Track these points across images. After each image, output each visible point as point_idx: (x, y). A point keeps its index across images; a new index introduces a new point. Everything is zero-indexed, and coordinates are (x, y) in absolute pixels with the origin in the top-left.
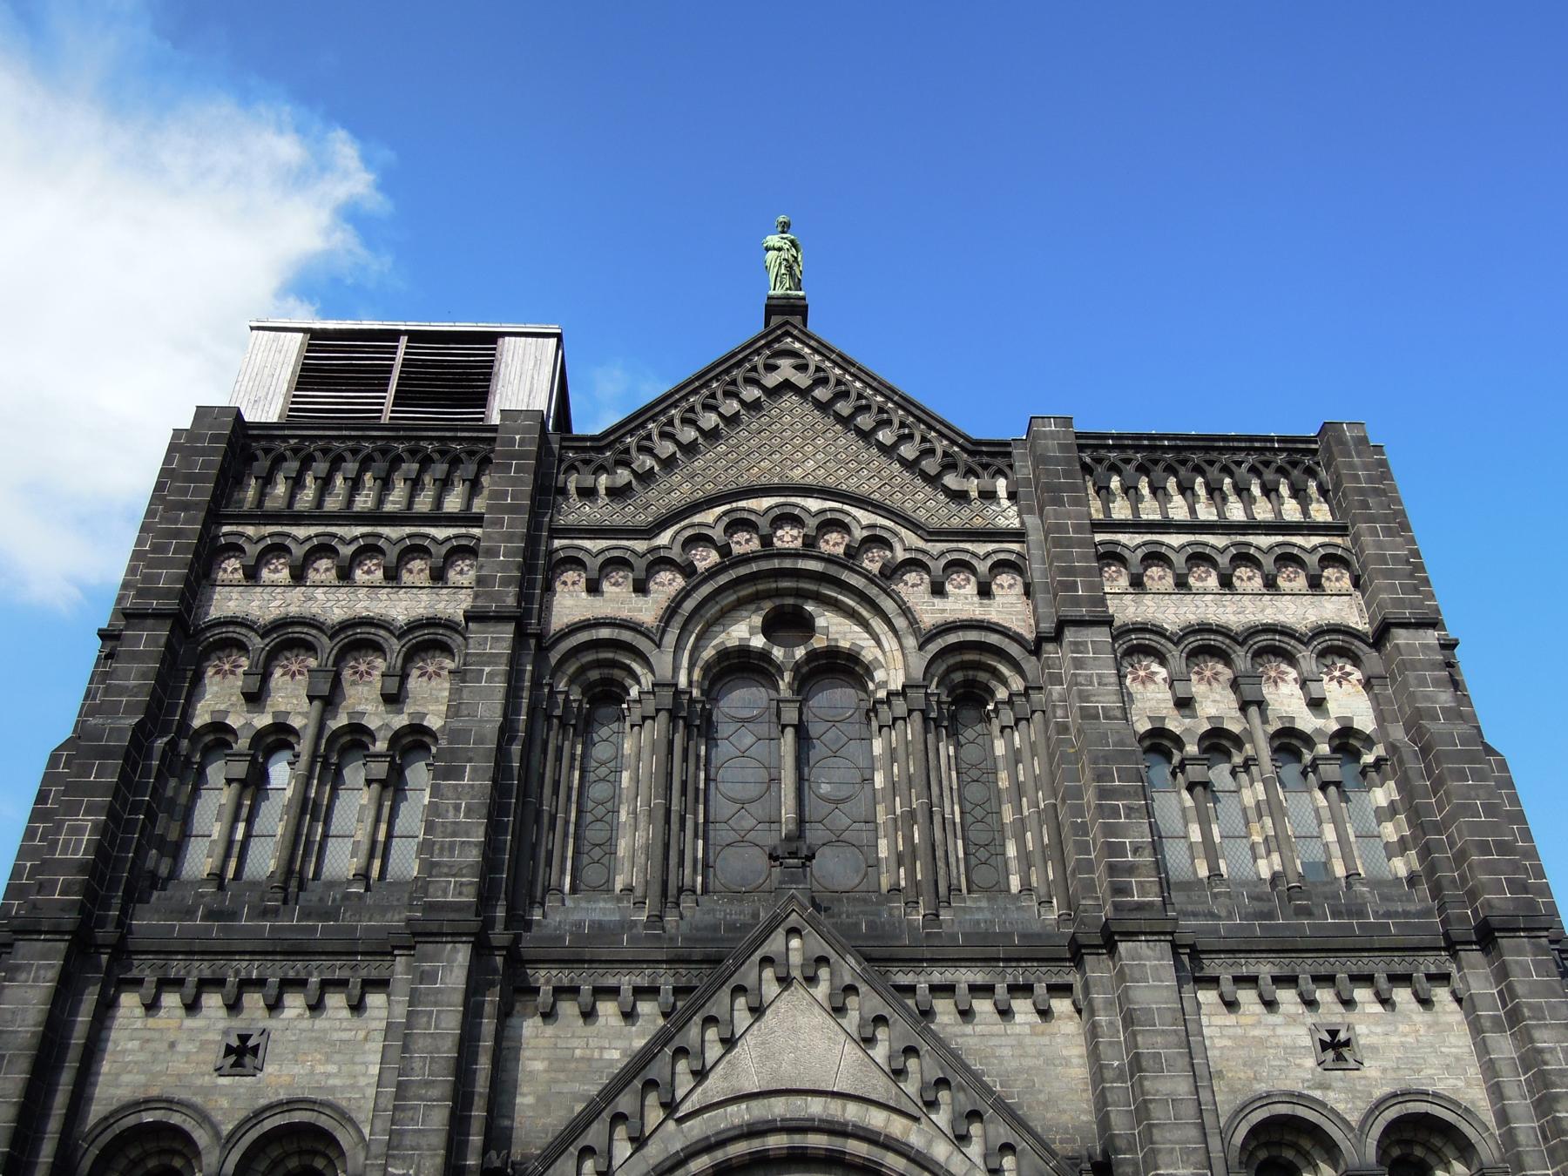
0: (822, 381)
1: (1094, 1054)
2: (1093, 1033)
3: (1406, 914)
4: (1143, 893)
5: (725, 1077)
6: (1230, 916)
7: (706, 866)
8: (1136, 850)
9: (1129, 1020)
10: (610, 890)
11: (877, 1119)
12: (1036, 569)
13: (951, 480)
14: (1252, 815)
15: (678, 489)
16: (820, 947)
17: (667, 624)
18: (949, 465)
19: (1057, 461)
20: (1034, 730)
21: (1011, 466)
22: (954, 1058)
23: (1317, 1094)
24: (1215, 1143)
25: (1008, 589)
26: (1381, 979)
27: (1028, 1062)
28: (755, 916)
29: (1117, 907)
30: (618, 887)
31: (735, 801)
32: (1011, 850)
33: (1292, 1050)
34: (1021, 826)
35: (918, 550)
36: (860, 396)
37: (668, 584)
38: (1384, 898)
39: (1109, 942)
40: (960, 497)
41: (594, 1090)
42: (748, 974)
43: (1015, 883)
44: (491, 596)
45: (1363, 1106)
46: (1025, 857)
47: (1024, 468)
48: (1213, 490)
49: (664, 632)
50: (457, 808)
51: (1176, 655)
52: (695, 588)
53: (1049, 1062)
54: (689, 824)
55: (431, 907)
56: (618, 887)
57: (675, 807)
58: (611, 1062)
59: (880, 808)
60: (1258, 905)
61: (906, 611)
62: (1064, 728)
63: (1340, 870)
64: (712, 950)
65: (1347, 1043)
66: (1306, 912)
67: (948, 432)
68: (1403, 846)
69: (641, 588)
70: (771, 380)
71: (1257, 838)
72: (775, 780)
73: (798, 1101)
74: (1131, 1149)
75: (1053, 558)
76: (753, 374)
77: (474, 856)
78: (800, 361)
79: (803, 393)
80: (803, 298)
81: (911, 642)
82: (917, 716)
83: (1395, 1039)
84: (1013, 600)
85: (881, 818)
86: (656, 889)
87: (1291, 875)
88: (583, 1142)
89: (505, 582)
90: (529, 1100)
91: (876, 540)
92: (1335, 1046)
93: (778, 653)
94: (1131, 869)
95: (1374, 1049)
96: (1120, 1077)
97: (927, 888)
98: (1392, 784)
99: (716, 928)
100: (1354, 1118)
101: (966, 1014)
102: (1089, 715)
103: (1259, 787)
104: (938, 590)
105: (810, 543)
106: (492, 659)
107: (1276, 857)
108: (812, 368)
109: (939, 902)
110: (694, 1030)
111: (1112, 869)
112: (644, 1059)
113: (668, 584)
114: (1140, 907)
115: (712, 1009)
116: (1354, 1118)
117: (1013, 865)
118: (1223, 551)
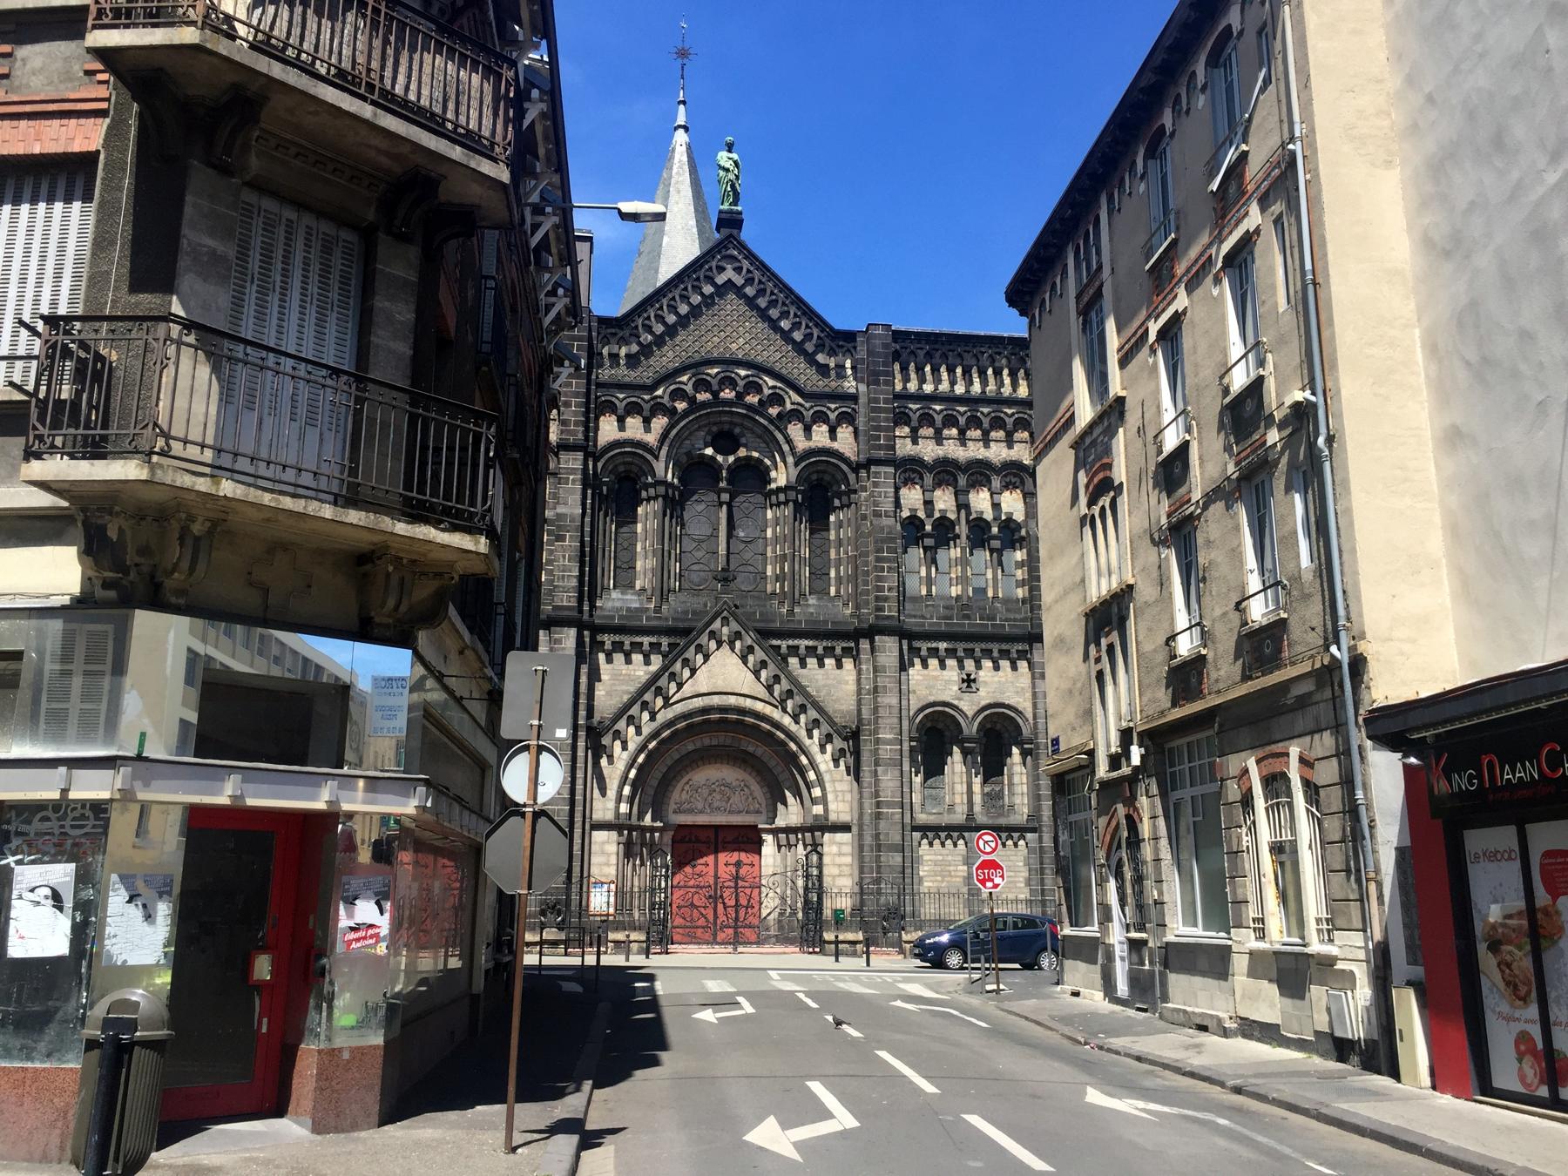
0: (749, 281)
1: (859, 681)
2: (859, 673)
3: (1015, 620)
4: (890, 611)
5: (693, 686)
6: (932, 618)
7: (680, 575)
8: (890, 589)
9: (876, 670)
10: (633, 587)
11: (759, 706)
12: (861, 421)
13: (821, 358)
14: (953, 563)
15: (667, 358)
16: (735, 626)
17: (662, 444)
18: (820, 347)
19: (879, 355)
20: (850, 512)
21: (855, 348)
22: (793, 680)
23: (956, 702)
24: (905, 724)
25: (844, 433)
26: (996, 654)
27: (830, 682)
28: (706, 605)
29: (877, 617)
30: (638, 587)
31: (694, 540)
32: (833, 574)
33: (948, 682)
34: (839, 562)
35: (799, 404)
36: (772, 293)
37: (660, 423)
38: (1007, 610)
39: (870, 633)
40: (823, 370)
41: (632, 689)
42: (704, 639)
43: (833, 591)
44: (570, 432)
45: (976, 708)
46: (839, 578)
47: (862, 352)
48: (967, 373)
49: (660, 449)
50: (564, 557)
51: (929, 479)
52: (678, 422)
53: (839, 682)
54: (673, 556)
55: (556, 608)
56: (638, 587)
57: (666, 548)
58: (639, 677)
59: (769, 549)
60: (947, 612)
61: (789, 441)
62: (864, 517)
63: (990, 594)
64: (686, 625)
65: (974, 680)
66: (967, 617)
67: (821, 323)
68: (1022, 584)
69: (647, 422)
70: (721, 279)
71: (953, 576)
72: (716, 529)
73: (725, 697)
74: (869, 724)
75: (871, 419)
76: (709, 273)
77: (574, 583)
78: (738, 264)
79: (739, 291)
80: (740, 213)
81: (790, 460)
82: (791, 504)
83: (996, 679)
84: (847, 435)
85: (769, 554)
86: (658, 593)
87: (965, 598)
88: (630, 713)
89: (576, 423)
90: (603, 693)
91: (776, 399)
92: (969, 682)
93: (720, 458)
94: (886, 599)
95: (985, 682)
96: (868, 694)
97: (789, 596)
98: (1025, 551)
99: (686, 612)
100: (970, 714)
101: (803, 664)
102: (877, 514)
103: (959, 550)
104: (808, 430)
105: (740, 396)
106: (573, 471)
107: (960, 587)
108: (745, 270)
109: (794, 602)
110: (678, 665)
111: (877, 599)
112: (656, 677)
113: (660, 423)
114: (888, 617)
115: (686, 655)
116: (970, 714)
117: (833, 582)
118: (962, 414)
